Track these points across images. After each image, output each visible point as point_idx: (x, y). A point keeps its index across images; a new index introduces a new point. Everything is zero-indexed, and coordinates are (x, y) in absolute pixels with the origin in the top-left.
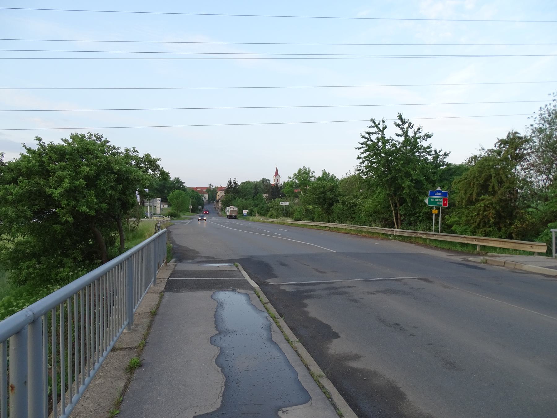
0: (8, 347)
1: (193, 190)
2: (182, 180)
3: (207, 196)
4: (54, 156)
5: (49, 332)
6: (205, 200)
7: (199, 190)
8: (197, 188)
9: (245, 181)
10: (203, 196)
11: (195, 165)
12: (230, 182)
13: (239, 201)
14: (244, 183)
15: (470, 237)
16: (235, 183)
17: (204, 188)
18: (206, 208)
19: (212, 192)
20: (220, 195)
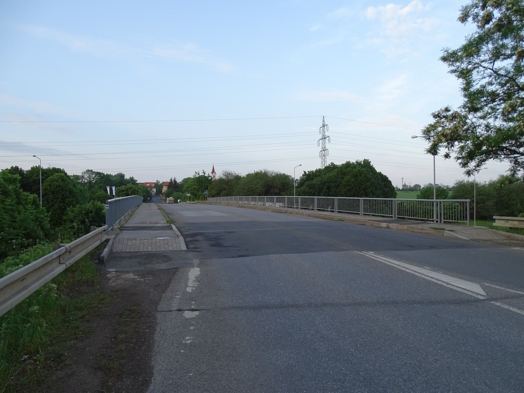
0: (234, 257)
1: (144, 185)
2: (135, 178)
3: (155, 190)
4: (507, 182)
5: (44, 266)
6: (153, 193)
7: (148, 185)
8: (147, 183)
9: (186, 177)
10: (151, 190)
11: (149, 167)
12: (171, 180)
13: (175, 194)
14: (186, 179)
15: (54, 254)
16: (175, 181)
17: (153, 183)
18: (153, 199)
19: (158, 186)
20: (165, 189)
